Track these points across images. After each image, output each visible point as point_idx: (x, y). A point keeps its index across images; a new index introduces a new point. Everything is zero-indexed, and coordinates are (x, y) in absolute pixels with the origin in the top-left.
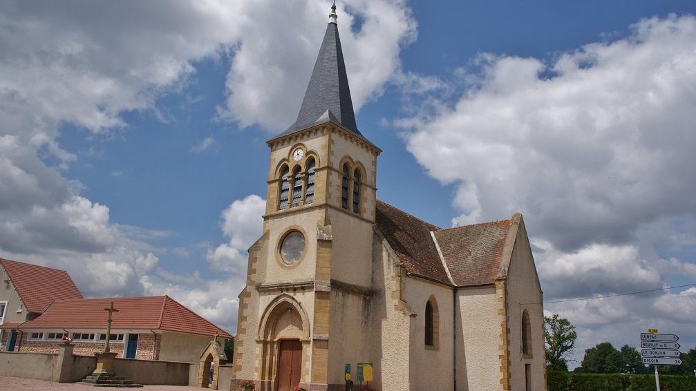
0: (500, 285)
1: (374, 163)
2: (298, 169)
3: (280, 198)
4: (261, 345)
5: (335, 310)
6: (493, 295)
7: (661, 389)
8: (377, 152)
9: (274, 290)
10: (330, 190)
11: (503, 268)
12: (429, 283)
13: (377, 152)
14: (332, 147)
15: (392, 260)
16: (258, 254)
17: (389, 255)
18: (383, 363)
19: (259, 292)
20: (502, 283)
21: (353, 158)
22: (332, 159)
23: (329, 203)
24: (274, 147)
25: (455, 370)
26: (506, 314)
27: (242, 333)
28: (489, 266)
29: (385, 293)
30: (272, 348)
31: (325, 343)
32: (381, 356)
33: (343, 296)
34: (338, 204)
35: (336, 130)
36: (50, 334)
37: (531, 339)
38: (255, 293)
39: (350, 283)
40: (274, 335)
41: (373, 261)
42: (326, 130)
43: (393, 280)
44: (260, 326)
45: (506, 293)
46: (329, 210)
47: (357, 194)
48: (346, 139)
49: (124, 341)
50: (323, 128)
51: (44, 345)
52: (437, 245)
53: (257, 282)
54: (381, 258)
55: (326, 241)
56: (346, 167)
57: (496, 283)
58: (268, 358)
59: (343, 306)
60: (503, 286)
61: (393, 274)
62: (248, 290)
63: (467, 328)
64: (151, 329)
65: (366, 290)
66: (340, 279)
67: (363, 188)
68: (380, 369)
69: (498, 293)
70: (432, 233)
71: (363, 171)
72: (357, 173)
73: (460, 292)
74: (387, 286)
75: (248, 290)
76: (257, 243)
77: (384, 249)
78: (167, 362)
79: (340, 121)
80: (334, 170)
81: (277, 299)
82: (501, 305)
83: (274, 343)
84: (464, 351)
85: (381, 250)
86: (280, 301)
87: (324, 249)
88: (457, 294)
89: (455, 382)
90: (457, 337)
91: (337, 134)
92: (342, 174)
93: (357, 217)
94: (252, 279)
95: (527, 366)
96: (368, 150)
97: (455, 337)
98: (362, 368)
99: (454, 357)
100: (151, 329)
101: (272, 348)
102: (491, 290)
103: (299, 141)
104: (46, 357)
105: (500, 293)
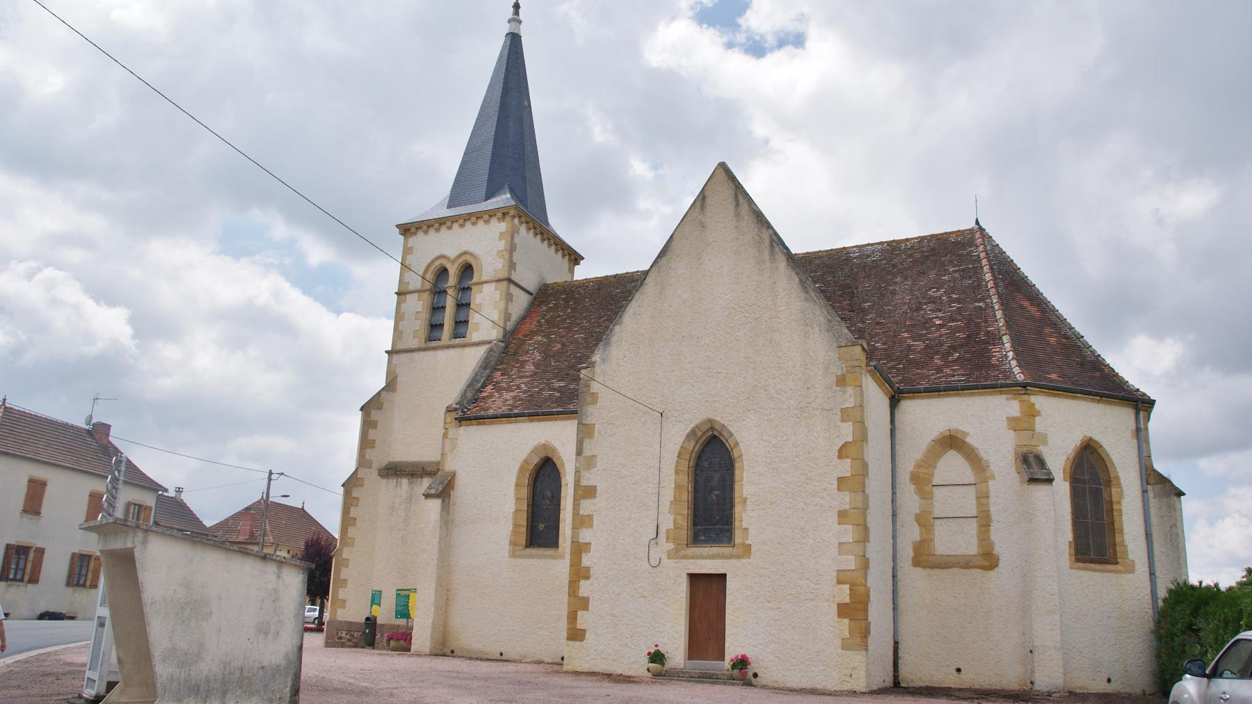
33: (410, 483)
71: (432, 269)
98: (408, 596)
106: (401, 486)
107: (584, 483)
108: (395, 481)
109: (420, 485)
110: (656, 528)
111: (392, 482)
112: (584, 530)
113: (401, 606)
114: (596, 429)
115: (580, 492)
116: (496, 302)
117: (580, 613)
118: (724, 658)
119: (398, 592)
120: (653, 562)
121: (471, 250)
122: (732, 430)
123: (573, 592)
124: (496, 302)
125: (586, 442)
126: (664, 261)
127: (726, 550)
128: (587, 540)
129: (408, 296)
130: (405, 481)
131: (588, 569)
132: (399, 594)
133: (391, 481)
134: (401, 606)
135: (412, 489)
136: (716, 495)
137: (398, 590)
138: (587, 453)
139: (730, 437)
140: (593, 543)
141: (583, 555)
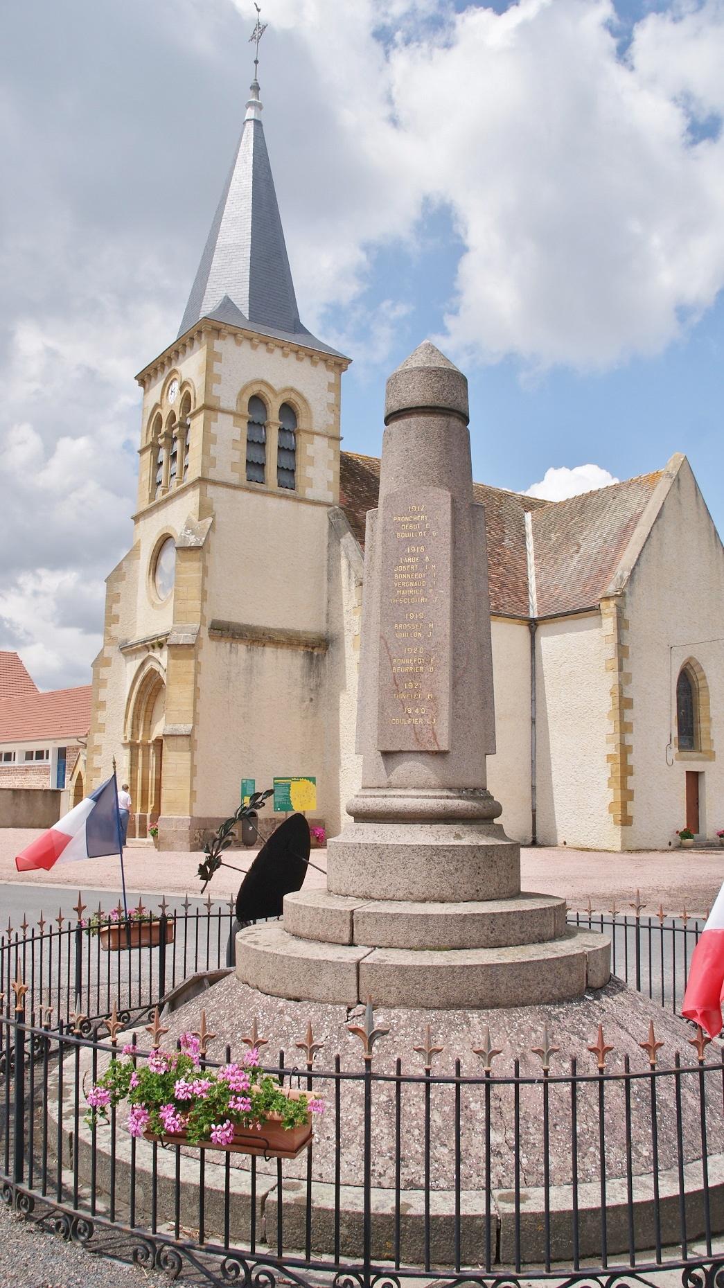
0: (609, 608)
1: (336, 387)
2: (172, 416)
3: (154, 478)
4: (128, 751)
5: (228, 679)
6: (597, 630)
7: (2, 768)
8: (340, 365)
9: (138, 650)
10: (212, 452)
11: (619, 574)
12: (573, 619)
13: (340, 365)
14: (217, 367)
15: (353, 573)
16: (121, 587)
17: (349, 566)
18: (342, 776)
19: (125, 655)
20: (612, 603)
21: (271, 382)
22: (217, 390)
23: (212, 475)
24: (147, 385)
25: (533, 788)
26: (620, 669)
27: (100, 731)
28: (603, 572)
29: (343, 642)
30: (146, 756)
31: (185, 742)
32: (339, 764)
33: (249, 651)
34: (238, 475)
35: (224, 332)
36: (27, 753)
37: (710, 720)
38: (118, 658)
39: (271, 625)
40: (148, 731)
41: (329, 580)
42: (203, 335)
43: (355, 613)
44: (126, 717)
45: (622, 623)
46: (211, 490)
47: (287, 451)
48: (254, 347)
49: (51, 762)
50: (200, 332)
51: (15, 771)
52: (530, 540)
53: (121, 638)
54: (338, 574)
55: (191, 549)
56: (257, 402)
57: (603, 605)
58: (152, 775)
59: (250, 670)
60: (614, 610)
61: (355, 601)
62: (106, 655)
63: (554, 701)
64: (77, 738)
65: (313, 636)
66: (224, 617)
67: (302, 439)
68: (338, 788)
69: (604, 627)
70: (528, 517)
71: (300, 402)
72: (288, 410)
73: (542, 629)
74: (347, 627)
75: (106, 655)
76: (119, 568)
77: (343, 553)
78: (14, 790)
79: (247, 316)
80: (224, 411)
81: (143, 664)
82: (610, 651)
83: (149, 745)
84: (548, 748)
85: (339, 555)
86: (147, 668)
87: (187, 564)
88: (537, 635)
89: (534, 811)
90: (537, 720)
91: (230, 342)
92: (242, 416)
93: (287, 497)
94: (113, 634)
95: (694, 779)
96: (314, 364)
97: (533, 722)
98: (289, 786)
99: (533, 762)
100: (77, 738)
101: (146, 756)
102: (591, 620)
103: (167, 371)
104: (11, 792)
105: (609, 624)
106: (237, 653)
107: (625, 695)
108: (228, 645)
109: (262, 654)
110: (669, 736)
111: (225, 646)
112: (628, 734)
113: (280, 797)
114: (630, 650)
115: (623, 703)
116: (330, 461)
117: (629, 803)
118: (193, 851)
119: (275, 781)
120: (670, 763)
121: (299, 388)
122: (703, 668)
123: (624, 786)
124: (330, 461)
125: (625, 661)
126: (660, 522)
127: (695, 755)
128: (630, 744)
129: (220, 415)
130: (242, 648)
131: (632, 766)
132: (277, 784)
133: (223, 644)
134: (280, 797)
135: (252, 658)
136: (683, 713)
137: (275, 779)
138: (626, 670)
139: (700, 672)
140: (634, 746)
141: (628, 755)
